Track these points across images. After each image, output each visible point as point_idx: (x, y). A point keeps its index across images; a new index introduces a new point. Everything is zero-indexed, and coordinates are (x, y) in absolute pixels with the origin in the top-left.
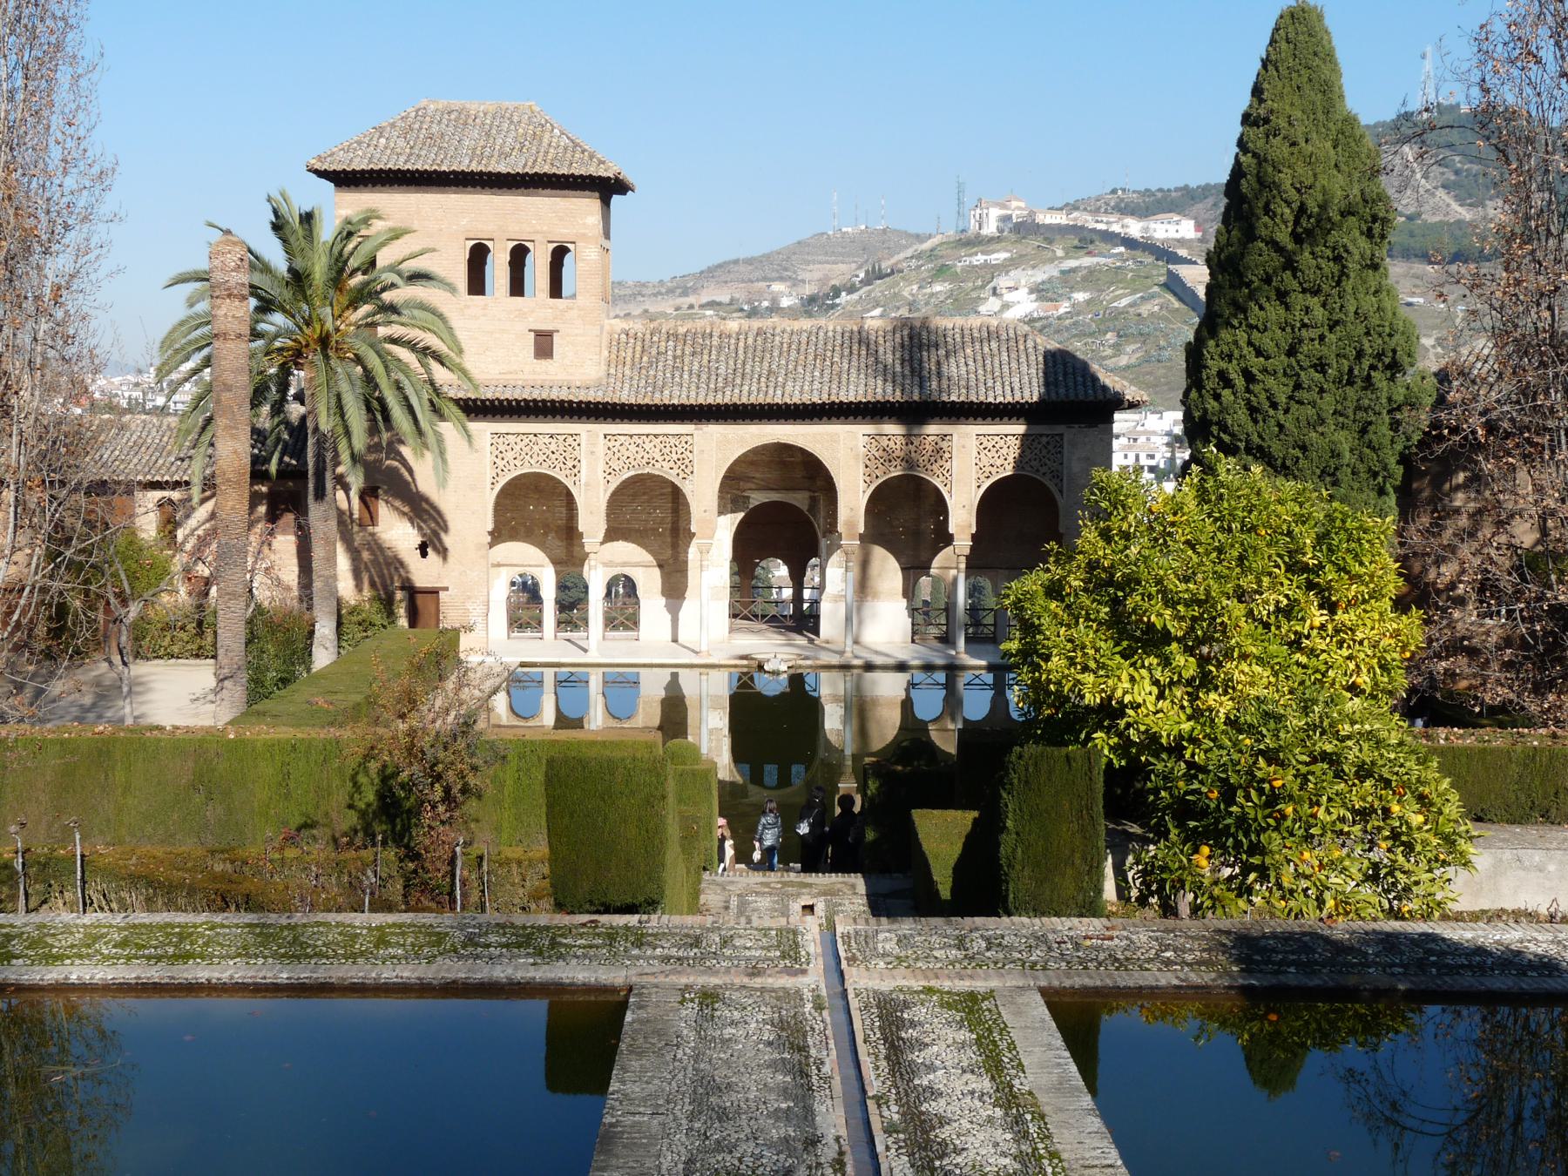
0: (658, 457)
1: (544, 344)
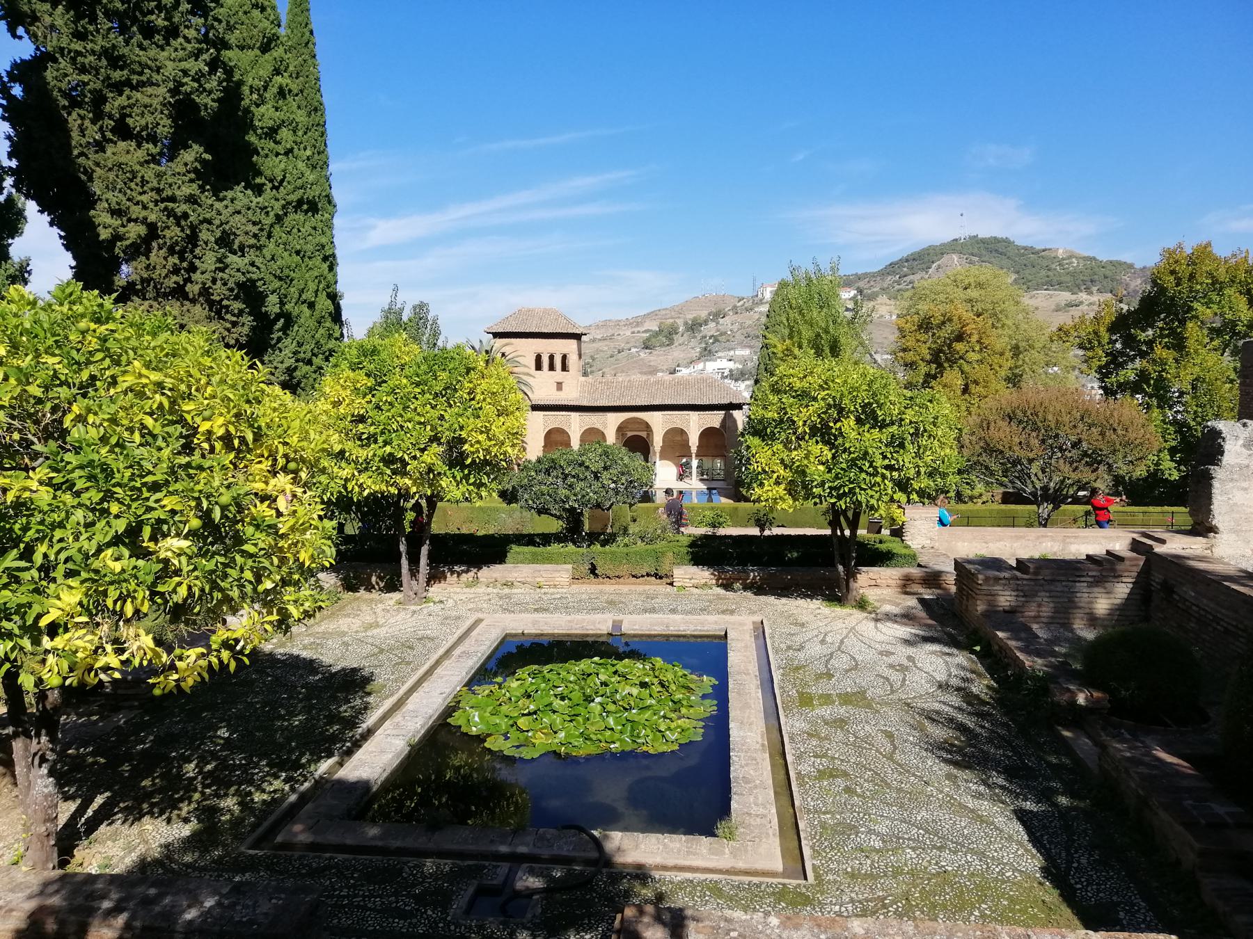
1: (559, 386)
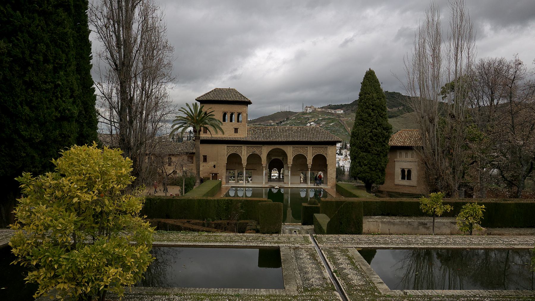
1: (236, 130)
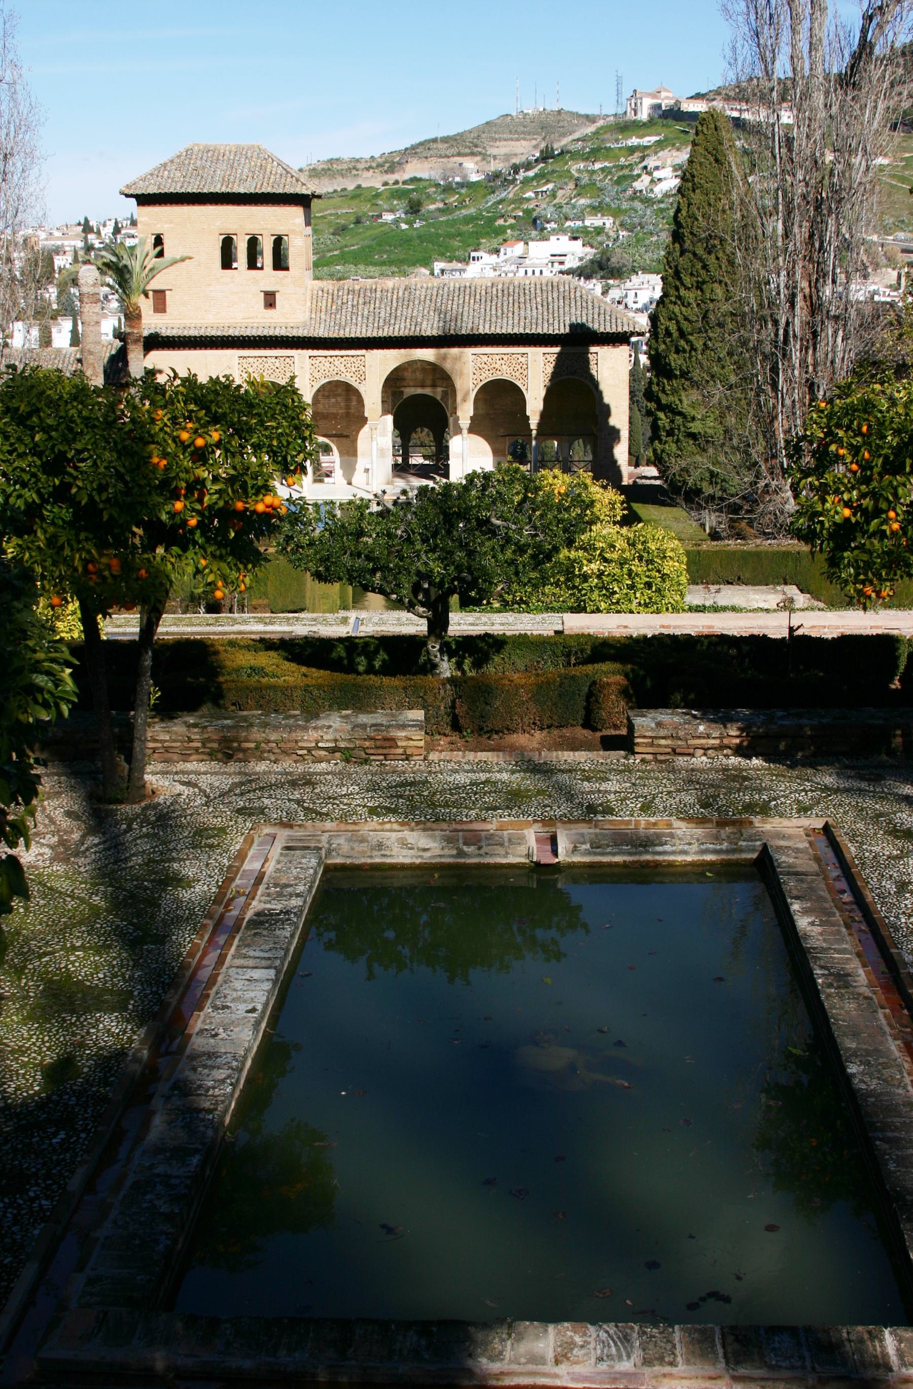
0: (343, 369)
1: (270, 300)
